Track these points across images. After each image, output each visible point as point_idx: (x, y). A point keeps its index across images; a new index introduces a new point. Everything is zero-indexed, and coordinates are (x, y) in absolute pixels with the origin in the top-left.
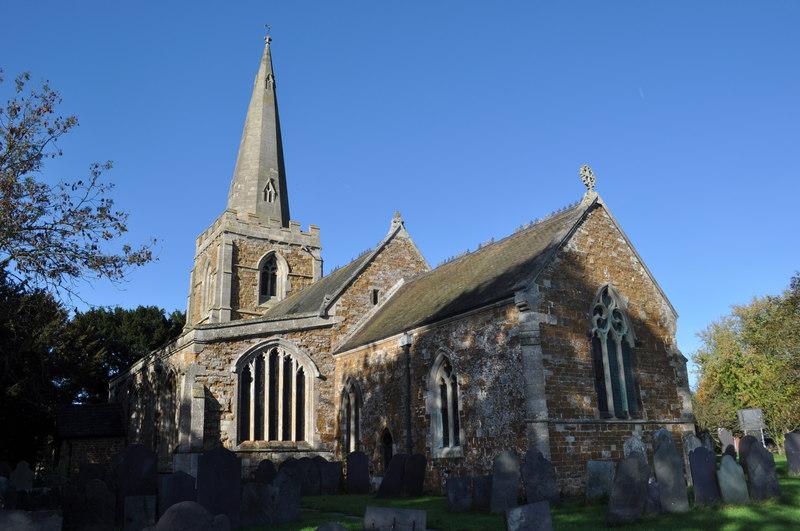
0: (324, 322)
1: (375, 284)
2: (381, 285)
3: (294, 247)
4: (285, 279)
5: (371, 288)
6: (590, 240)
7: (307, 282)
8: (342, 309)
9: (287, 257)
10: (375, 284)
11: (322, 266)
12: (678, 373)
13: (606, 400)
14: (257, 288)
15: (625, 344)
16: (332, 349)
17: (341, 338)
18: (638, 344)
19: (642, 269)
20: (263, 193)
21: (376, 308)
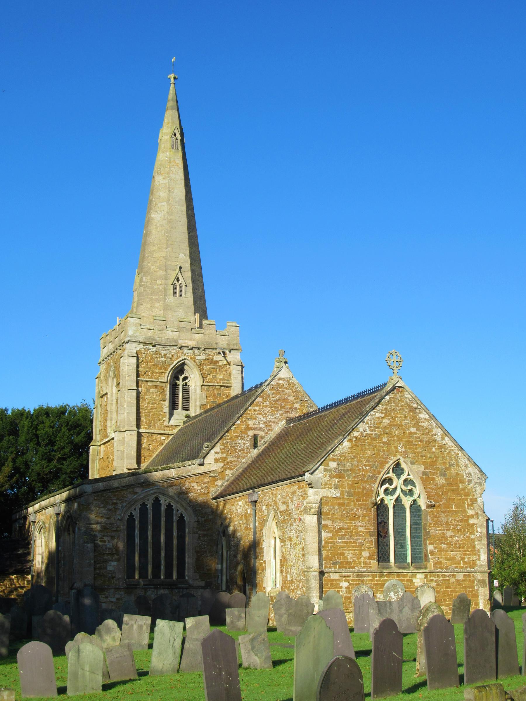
0: (202, 469)
1: (255, 429)
2: (261, 429)
3: (208, 352)
4: (198, 391)
5: (251, 433)
6: (386, 421)
7: (225, 391)
8: (219, 456)
9: (200, 365)
10: (255, 429)
11: (242, 372)
12: (479, 529)
13: (166, 554)
14: (167, 403)
15: (414, 506)
16: (211, 495)
17: (219, 483)
18: (431, 506)
19: (447, 439)
20: (172, 287)
21: (255, 452)
